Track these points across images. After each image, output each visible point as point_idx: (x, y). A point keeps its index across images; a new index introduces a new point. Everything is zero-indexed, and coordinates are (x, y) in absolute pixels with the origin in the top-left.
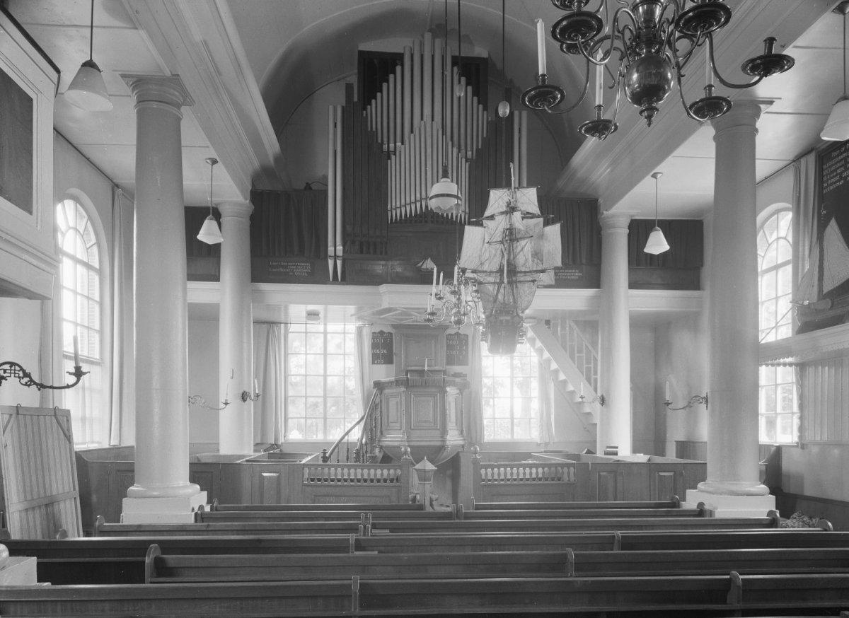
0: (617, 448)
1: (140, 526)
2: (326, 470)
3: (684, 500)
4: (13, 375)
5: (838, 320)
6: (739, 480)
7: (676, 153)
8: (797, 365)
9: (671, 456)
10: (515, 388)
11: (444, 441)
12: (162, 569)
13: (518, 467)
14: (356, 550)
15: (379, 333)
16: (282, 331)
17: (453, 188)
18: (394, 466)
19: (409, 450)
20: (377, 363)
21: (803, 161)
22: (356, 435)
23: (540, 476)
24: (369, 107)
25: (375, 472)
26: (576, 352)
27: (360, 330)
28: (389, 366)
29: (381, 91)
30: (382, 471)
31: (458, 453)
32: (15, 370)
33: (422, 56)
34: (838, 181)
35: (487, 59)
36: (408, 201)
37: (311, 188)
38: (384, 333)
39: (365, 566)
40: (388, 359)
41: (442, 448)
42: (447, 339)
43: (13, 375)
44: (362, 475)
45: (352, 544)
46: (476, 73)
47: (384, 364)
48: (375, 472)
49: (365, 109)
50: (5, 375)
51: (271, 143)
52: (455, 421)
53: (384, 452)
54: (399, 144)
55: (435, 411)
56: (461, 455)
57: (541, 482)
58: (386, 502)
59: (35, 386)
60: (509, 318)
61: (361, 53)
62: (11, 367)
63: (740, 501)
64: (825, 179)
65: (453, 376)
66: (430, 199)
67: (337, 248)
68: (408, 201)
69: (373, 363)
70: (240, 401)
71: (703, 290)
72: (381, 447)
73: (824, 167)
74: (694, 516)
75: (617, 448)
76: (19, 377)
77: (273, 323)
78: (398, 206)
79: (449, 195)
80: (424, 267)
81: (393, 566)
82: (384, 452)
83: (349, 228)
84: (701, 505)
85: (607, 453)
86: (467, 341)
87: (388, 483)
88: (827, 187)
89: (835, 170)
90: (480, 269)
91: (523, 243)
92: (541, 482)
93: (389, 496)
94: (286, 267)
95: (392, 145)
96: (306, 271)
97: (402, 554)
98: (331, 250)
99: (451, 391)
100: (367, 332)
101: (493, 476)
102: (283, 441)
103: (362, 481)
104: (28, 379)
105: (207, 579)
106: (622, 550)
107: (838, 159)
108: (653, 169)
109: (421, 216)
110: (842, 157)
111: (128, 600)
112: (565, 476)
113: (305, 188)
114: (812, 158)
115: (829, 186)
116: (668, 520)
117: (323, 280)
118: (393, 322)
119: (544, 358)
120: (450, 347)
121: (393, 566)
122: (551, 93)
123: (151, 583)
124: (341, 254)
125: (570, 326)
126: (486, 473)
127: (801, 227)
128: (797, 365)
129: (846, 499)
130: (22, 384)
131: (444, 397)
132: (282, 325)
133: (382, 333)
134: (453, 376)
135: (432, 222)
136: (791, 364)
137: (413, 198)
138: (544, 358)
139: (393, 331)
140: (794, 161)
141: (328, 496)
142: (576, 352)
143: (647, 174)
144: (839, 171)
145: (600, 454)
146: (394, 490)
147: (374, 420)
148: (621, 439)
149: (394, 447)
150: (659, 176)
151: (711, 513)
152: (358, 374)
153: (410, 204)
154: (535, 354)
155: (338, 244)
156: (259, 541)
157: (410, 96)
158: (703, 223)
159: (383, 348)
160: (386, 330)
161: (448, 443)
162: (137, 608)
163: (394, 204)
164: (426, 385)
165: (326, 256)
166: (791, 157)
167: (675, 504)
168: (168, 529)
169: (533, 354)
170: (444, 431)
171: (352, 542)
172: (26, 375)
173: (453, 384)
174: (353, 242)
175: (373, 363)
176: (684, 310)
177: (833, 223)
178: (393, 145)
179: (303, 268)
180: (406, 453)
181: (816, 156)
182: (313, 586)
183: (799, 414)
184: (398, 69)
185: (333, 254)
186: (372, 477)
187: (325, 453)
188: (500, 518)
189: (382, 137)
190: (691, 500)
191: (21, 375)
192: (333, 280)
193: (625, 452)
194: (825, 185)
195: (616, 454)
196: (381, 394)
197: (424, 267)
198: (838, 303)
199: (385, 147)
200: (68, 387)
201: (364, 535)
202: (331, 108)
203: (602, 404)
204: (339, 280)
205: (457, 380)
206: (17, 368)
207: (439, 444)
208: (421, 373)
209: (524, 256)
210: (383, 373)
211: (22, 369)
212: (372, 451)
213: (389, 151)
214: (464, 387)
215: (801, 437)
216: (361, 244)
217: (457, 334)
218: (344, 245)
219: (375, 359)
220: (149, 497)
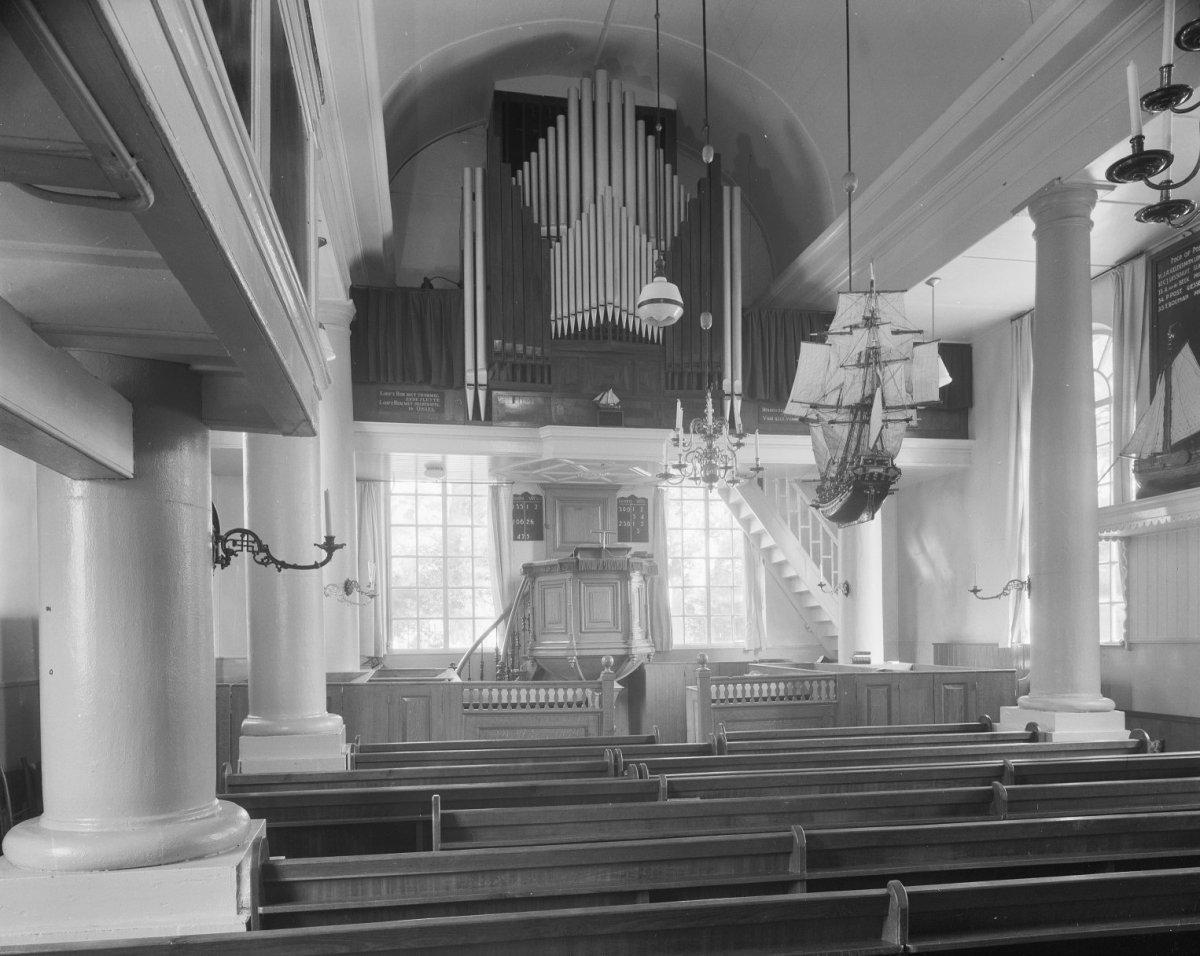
0: (869, 653)
1: (289, 776)
2: (485, 692)
3: (998, 721)
4: (245, 548)
5: (1188, 482)
6: (1076, 692)
7: (966, 253)
8: (1122, 539)
9: (927, 661)
12: (454, 832)
13: (744, 681)
14: (669, 798)
16: (382, 492)
17: (673, 291)
18: (555, 684)
19: (612, 660)
20: (521, 539)
21: (1127, 267)
22: (495, 642)
23: (782, 693)
24: (520, 172)
25: (537, 692)
26: (800, 523)
27: (495, 490)
28: (538, 543)
29: (537, 150)
30: (769, 685)
32: (247, 541)
33: (594, 104)
34: (1181, 296)
35: (675, 111)
36: (579, 309)
37: (431, 287)
38: (530, 495)
39: (729, 816)
40: (537, 533)
42: (618, 505)
43: (245, 548)
44: (547, 697)
45: (664, 789)
46: (663, 128)
47: (531, 539)
48: (744, 688)
49: (514, 174)
50: (235, 548)
51: (385, 221)
53: (539, 666)
54: (563, 228)
55: (615, 606)
56: (647, 667)
57: (792, 702)
58: (580, 734)
59: (273, 565)
60: (881, 470)
61: (498, 94)
62: (242, 537)
63: (1088, 725)
64: (1160, 292)
66: (640, 306)
67: (479, 373)
68: (579, 309)
69: (515, 539)
70: (342, 592)
71: (974, 438)
72: (535, 659)
73: (1160, 276)
74: (1025, 741)
75: (869, 653)
76: (253, 552)
77: (369, 480)
78: (565, 313)
79: (667, 301)
80: (603, 401)
81: (768, 814)
82: (539, 666)
84: (1032, 726)
85: (856, 662)
86: (646, 508)
87: (565, 709)
88: (1163, 303)
89: (1177, 281)
90: (822, 403)
91: (893, 367)
92: (792, 702)
93: (585, 727)
94: (402, 399)
95: (553, 229)
96: (432, 405)
97: (782, 798)
98: (470, 377)
99: (636, 579)
100: (505, 496)
101: (778, 694)
102: (386, 652)
103: (509, 707)
104: (265, 555)
105: (512, 842)
106: (1016, 784)
107: (1179, 267)
108: (931, 273)
109: (598, 329)
110: (1186, 264)
111: (483, 871)
112: (815, 694)
113: (423, 286)
114: (1140, 265)
115: (1166, 302)
116: (964, 749)
118: (545, 479)
119: (752, 532)
120: (622, 516)
121: (768, 814)
122: (1155, 159)
123: (442, 850)
124: (485, 382)
125: (791, 487)
126: (727, 690)
127: (1126, 357)
128: (1122, 539)
129: (1196, 714)
130: (258, 562)
131: (626, 586)
133: (526, 495)
135: (614, 338)
136: (1115, 538)
137: (594, 302)
138: (752, 532)
139: (540, 492)
140: (1114, 268)
141: (498, 728)
142: (800, 523)
143: (920, 280)
144: (1181, 283)
145: (844, 661)
146: (591, 717)
148: (871, 645)
149: (557, 658)
150: (936, 282)
151: (1046, 737)
152: (494, 555)
153: (583, 312)
154: (739, 526)
155: (479, 367)
156: (533, 788)
157: (577, 160)
158: (971, 348)
159: (530, 515)
162: (496, 882)
163: (559, 312)
164: (603, 569)
165: (462, 386)
166: (1111, 262)
167: (986, 726)
168: (329, 779)
169: (737, 524)
170: (628, 634)
171: (664, 785)
172: (264, 549)
174: (502, 365)
175: (515, 539)
176: (925, 465)
177: (1186, 352)
178: (546, 228)
179: (429, 399)
180: (607, 665)
181: (1147, 263)
182: (742, 841)
183: (1124, 605)
184: (561, 118)
185: (473, 382)
186: (561, 700)
188: (672, 754)
189: (539, 218)
190: (1011, 721)
191: (256, 549)
192: (486, 419)
193: (878, 661)
194: (1161, 300)
195: (869, 662)
196: (533, 582)
197: (603, 401)
198: (1182, 464)
199: (544, 229)
200: (316, 566)
201: (641, 777)
202: (467, 171)
203: (846, 595)
204: (470, 418)
205: (644, 562)
206: (251, 538)
207: (622, 652)
208: (597, 552)
209: (895, 384)
210: (527, 552)
211: (257, 539)
212: (520, 662)
213: (549, 236)
215: (1127, 635)
216: (514, 366)
217: (633, 498)
218: (489, 366)
219: (518, 532)
220: (279, 734)
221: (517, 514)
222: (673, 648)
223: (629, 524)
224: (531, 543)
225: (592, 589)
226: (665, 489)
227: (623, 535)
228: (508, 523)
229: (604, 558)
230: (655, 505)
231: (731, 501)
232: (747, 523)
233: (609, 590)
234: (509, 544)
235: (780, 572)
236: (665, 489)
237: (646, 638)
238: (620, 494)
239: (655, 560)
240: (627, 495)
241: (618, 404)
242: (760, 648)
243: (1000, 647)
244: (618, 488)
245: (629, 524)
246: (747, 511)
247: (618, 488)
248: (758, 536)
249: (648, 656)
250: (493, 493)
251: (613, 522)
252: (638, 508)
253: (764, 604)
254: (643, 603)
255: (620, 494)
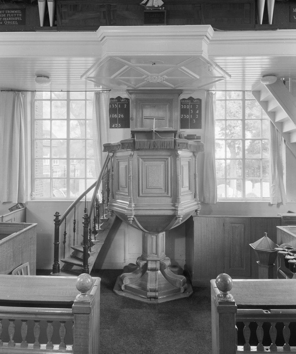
10: (227, 148)
11: (175, 210)
15: (117, 98)
20: (115, 128)
27: (98, 95)
28: (126, 129)
31: (191, 217)
38: (121, 98)
40: (125, 123)
41: (173, 217)
47: (121, 127)
52: (188, 185)
65: (186, 138)
69: (111, 127)
83: (233, 204)
117: (34, 27)
120: (183, 111)
132: (29, 94)
133: (119, 98)
134: (186, 138)
147: (108, 180)
160: (125, 95)
161: (179, 213)
169: (266, 116)
170: (175, 199)
173: (186, 146)
187: (57, 215)
192: (54, 25)
204: (42, 25)
205: (190, 142)
207: (170, 213)
210: (119, 135)
214: (197, 150)
217: (191, 99)
219: (113, 123)
221: (112, 111)
222: (218, 201)
223: (188, 117)
224: (122, 129)
225: (147, 163)
226: (214, 92)
227: (184, 124)
228: (107, 116)
229: (154, 140)
230: (207, 103)
231: (269, 110)
232: (273, 114)
233: (162, 164)
234: (107, 131)
235: (282, 128)
236: (214, 92)
237: (195, 197)
238: (182, 97)
239: (202, 141)
240: (187, 97)
241: (162, 6)
242: (282, 203)
243: (197, 136)
244: (180, 92)
245: (188, 117)
246: (274, 104)
247: (180, 92)
248: (281, 124)
249: (196, 211)
250: (96, 97)
251: (177, 115)
252: (194, 106)
253: (284, 171)
254: (192, 174)
255: (182, 97)
